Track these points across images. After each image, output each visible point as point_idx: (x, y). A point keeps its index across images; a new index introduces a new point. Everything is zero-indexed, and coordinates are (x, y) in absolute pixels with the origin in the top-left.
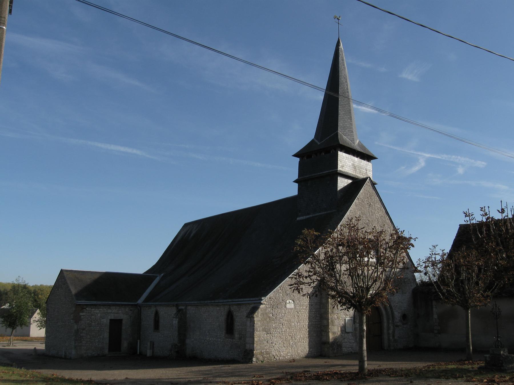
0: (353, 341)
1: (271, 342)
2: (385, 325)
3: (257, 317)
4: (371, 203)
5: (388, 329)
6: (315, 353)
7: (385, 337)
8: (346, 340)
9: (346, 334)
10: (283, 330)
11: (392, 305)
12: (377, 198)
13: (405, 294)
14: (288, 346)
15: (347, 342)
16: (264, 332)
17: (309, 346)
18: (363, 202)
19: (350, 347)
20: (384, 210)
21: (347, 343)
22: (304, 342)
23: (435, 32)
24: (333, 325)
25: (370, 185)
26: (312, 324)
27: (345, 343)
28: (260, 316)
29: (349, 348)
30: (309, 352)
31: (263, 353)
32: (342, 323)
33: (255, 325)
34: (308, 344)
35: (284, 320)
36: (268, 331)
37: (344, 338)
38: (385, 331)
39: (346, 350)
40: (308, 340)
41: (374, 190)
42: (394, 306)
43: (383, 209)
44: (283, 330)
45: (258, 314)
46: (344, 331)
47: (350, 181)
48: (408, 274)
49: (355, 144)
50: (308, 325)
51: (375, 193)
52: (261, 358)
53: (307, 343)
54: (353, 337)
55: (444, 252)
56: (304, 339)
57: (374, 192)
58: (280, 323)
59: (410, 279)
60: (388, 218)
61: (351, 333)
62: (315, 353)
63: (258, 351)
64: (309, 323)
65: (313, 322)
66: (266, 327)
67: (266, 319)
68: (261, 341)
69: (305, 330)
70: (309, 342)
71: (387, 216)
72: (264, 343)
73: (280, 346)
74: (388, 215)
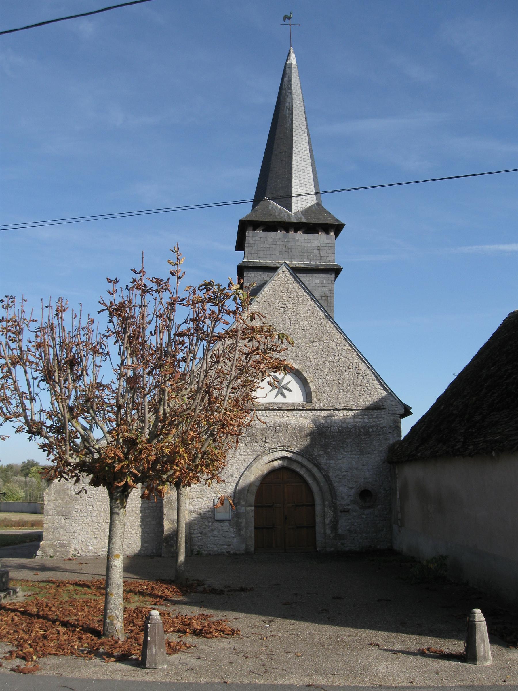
0: (233, 535)
1: (72, 530)
2: (318, 509)
3: (48, 495)
4: (289, 305)
5: (324, 516)
6: (154, 551)
7: (319, 529)
8: (215, 533)
9: (216, 524)
10: (94, 514)
11: (330, 474)
12: (305, 294)
13: (369, 455)
14: (102, 538)
15: (219, 536)
16: (60, 517)
17: (141, 538)
18: (270, 306)
19: (224, 543)
20: (321, 312)
21: (217, 537)
22: (133, 532)
23: (114, 9)
24: (172, 509)
25: (288, 275)
26: (149, 506)
27: (214, 537)
28: (53, 494)
29: (223, 545)
30: (142, 548)
31: (56, 545)
32: (208, 506)
33: (45, 507)
34: (140, 537)
35: (96, 500)
36: (67, 514)
37: (212, 530)
38: (318, 519)
39: (216, 549)
40: (140, 530)
41: (298, 282)
42: (336, 477)
43: (318, 311)
44: (94, 514)
45: (50, 491)
46: (211, 518)
47: (297, 274)
48: (382, 418)
49: (292, 212)
50: (141, 507)
51: (300, 287)
52: (51, 552)
53: (139, 534)
54: (233, 528)
55: (112, 384)
56: (133, 528)
57: (298, 285)
58: (88, 504)
59: (384, 427)
60: (332, 325)
61: (228, 522)
62: (154, 551)
63: (49, 542)
64: (142, 504)
65: (150, 504)
66: (64, 509)
67: (63, 499)
68: (54, 528)
69: (135, 515)
70: (143, 533)
71: (330, 322)
72: (59, 532)
73: (88, 537)
74: (330, 320)
